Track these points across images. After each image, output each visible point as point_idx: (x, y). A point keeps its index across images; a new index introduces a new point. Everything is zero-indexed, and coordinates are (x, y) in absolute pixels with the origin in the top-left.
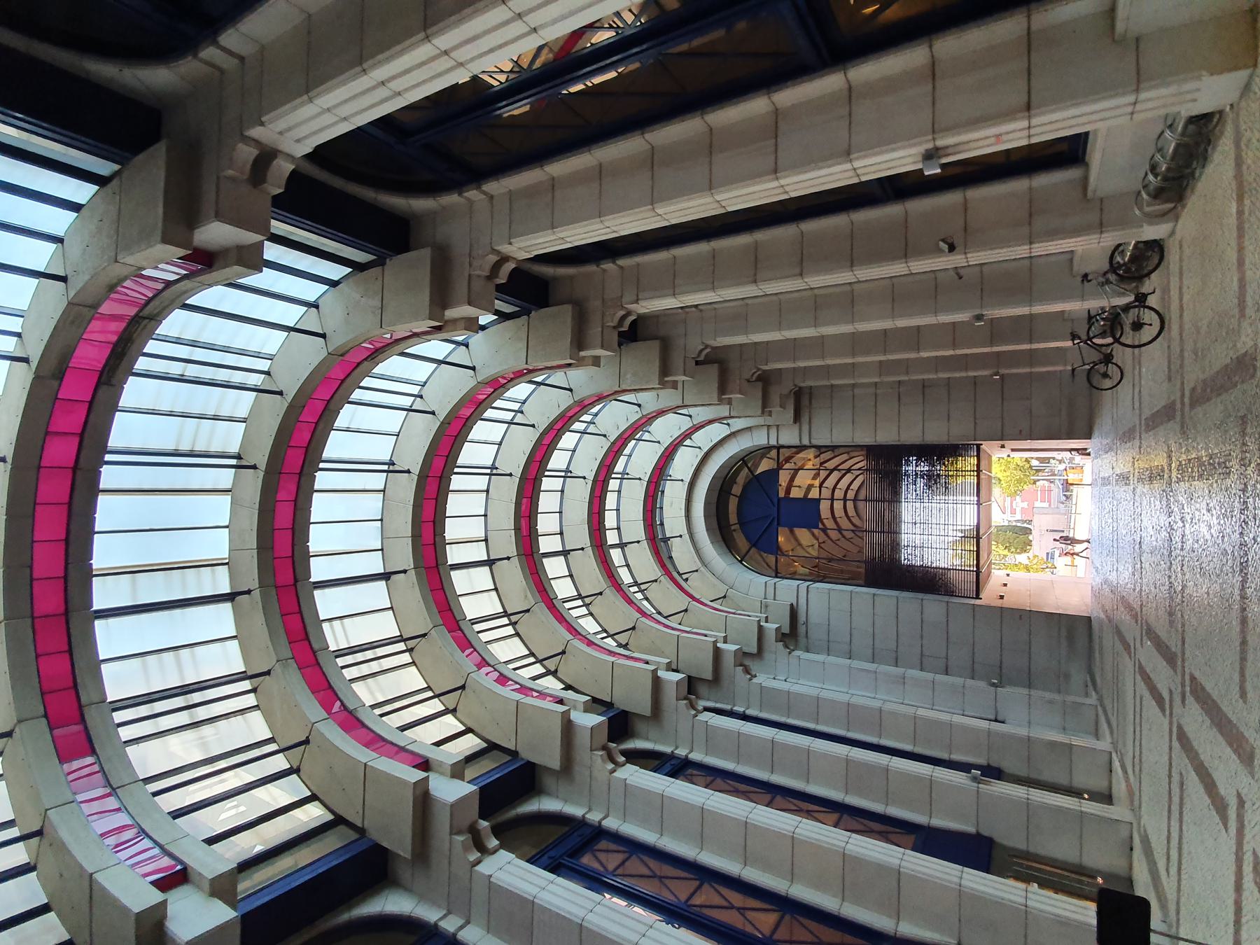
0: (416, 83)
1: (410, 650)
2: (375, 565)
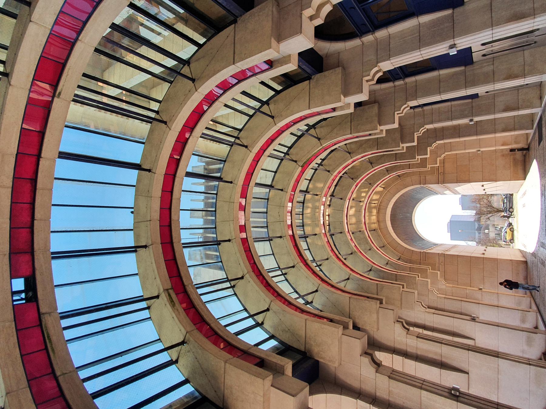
1: (233, 287)
2: (128, 240)
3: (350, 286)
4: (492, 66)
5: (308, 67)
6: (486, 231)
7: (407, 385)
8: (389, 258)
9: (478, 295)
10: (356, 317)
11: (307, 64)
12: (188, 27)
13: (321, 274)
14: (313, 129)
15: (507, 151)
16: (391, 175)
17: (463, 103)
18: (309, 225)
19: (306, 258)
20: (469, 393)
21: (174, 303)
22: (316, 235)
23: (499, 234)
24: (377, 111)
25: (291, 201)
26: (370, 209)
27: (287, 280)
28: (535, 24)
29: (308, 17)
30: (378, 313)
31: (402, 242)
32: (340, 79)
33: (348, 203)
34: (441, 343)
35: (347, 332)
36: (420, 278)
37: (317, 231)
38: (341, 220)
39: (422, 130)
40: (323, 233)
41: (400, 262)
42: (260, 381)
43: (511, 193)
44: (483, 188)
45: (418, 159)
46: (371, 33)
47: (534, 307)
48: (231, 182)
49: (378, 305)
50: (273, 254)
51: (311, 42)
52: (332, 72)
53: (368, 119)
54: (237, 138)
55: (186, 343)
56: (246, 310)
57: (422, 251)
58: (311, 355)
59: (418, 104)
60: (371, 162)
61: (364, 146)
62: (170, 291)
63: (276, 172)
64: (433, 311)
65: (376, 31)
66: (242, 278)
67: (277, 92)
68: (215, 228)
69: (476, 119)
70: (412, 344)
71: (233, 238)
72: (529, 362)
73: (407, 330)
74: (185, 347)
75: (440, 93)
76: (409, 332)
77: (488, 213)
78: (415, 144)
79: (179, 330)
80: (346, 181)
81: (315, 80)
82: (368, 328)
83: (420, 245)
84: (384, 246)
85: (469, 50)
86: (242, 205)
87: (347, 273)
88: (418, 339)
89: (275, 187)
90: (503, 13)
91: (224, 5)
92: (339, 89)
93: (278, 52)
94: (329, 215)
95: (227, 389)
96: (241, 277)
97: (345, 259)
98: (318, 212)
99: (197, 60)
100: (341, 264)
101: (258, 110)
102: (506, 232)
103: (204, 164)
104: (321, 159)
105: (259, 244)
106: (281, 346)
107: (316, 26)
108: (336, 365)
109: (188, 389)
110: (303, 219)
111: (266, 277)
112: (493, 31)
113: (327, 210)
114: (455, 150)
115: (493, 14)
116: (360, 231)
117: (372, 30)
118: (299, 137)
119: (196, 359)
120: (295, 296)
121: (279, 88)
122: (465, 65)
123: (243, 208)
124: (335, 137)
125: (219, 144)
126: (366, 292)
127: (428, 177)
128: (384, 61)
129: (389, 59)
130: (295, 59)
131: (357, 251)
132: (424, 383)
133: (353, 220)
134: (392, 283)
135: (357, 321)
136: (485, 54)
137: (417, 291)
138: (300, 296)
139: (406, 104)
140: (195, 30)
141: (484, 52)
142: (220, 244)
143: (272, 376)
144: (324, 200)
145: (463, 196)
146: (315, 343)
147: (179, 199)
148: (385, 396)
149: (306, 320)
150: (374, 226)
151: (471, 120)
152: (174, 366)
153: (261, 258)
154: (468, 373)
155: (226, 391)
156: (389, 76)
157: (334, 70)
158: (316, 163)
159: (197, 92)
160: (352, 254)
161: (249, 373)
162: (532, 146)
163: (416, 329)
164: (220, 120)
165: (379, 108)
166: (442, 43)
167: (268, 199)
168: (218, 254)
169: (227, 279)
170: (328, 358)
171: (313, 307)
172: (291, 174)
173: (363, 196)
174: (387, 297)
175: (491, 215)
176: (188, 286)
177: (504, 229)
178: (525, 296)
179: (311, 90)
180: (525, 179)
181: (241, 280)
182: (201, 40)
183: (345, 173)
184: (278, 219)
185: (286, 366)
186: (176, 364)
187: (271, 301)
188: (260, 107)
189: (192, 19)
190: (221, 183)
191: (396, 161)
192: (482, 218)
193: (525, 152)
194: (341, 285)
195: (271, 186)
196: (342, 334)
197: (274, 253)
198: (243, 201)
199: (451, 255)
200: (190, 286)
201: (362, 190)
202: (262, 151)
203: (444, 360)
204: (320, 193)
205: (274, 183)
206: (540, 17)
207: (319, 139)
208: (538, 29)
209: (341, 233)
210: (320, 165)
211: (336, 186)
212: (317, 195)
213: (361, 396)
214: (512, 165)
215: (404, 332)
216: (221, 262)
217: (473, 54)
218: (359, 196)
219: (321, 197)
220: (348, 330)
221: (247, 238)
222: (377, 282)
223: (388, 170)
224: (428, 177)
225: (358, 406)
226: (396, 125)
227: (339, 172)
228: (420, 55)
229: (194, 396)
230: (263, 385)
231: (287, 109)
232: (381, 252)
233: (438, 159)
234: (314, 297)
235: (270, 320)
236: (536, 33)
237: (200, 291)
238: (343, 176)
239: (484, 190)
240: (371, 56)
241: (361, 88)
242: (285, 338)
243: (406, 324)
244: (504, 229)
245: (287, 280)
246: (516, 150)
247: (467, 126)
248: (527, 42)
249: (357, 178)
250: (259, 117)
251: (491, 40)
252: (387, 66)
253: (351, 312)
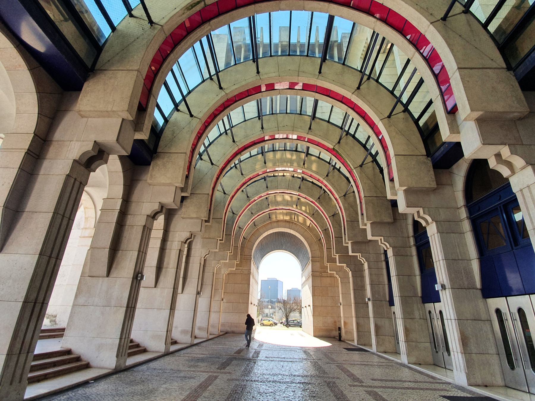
0: (484, 70)
1: (211, 78)
3: (218, 194)
4: (419, 318)
5: (442, 153)
6: (270, 307)
7: (140, 240)
8: (245, 230)
9: (217, 298)
10: (192, 200)
11: (444, 153)
12: (511, 10)
13: (228, 168)
14: (372, 160)
15: (339, 325)
16: (322, 233)
17: (386, 294)
18: (275, 156)
19: (242, 153)
20: (140, 287)
21: (191, 9)
22: (265, 163)
23: (267, 316)
24: (385, 221)
25: (299, 138)
26: (290, 214)
27: (221, 135)
28: (456, 353)
29: (500, 152)
30: (197, 218)
31: (259, 241)
32: (425, 186)
33: (295, 193)
34: (177, 268)
35: (179, 191)
36: (229, 254)
37: (269, 164)
38: (279, 187)
39: (363, 260)
40: (267, 170)
41: (241, 239)
42: (126, 107)
43: (302, 326)
44: (307, 306)
45: (336, 256)
46: (468, 216)
47: (211, 337)
48: (320, 72)
49: (204, 219)
50: (245, 121)
51: (471, 154)
52: (432, 178)
53: (378, 213)
54: (369, 77)
55: (152, 26)
56: (189, 92)
57: (252, 257)
58: (154, 158)
59: (388, 257)
60: (334, 216)
61: (351, 209)
62: (203, 3)
63: (328, 122)
64: (202, 263)
65: (470, 221)
66: (221, 88)
67: (416, 121)
68: (271, 56)
69: (370, 304)
70: (173, 245)
71: (260, 76)
72: (169, 331)
73: (185, 242)
74: (147, 25)
75: (398, 275)
76: (183, 244)
77: (285, 308)
78: (350, 253)
79: (164, 16)
80: (317, 193)
81: (425, 160)
82: (183, 210)
83: (257, 256)
84: (255, 225)
85: (437, 300)
86: (294, 86)
87: (229, 193)
88: (179, 251)
89: (313, 122)
90: (469, 329)
91: (532, 55)
92: (414, 185)
93: (465, 119)
94: (284, 176)
95: (113, 73)
96: (222, 86)
97: (242, 191)
98: (287, 165)
99: (468, 22)
100: (238, 187)
101: (399, 100)
102: (269, 321)
103: (339, 41)
104: (340, 167)
105: (255, 106)
106: (159, 130)
107: (488, 161)
108: (149, 181)
109: (106, 31)
110: (279, 150)
111: (223, 113)
112: (454, 320)
113: (288, 174)
114: (342, 286)
115: (471, 321)
116: (269, 205)
117: (471, 217)
118: (364, 146)
119: (136, 38)
120: (207, 143)
121: (421, 123)
122: (422, 297)
123: (292, 86)
124: (362, 182)
125: (361, 58)
126: (214, 209)
127: (318, 264)
128: (437, 228)
129: (438, 231)
130: (454, 139)
131: (250, 201)
132: (144, 254)
133: (279, 199)
134: (223, 231)
135: (188, 201)
136: (431, 313)
137: (218, 251)
138: (206, 148)
139: (390, 246)
140: (506, 19)
141: (433, 312)
142: (254, 62)
143: (132, 119)
144: (299, 171)
145: (299, 291)
146: (165, 162)
147: (304, 9)
148: (128, 222)
149: (185, 153)
150: (274, 217)
151: (369, 299)
152: (126, 13)
153: (241, 108)
154: (155, 287)
155: (111, 72)
156: (420, 232)
157: (434, 180)
158: (336, 163)
159: (429, 23)
160: (248, 197)
161: (131, 97)
162: (342, 343)
163: (186, 250)
164: (390, 58)
165: (389, 223)
166: (448, 278)
167: (301, 114)
168: (242, 61)
169: (218, 71)
170: (154, 173)
171: (197, 161)
172: (326, 138)
173: (302, 208)
174: (211, 226)
175: (284, 311)
176: (209, 25)
177: (272, 320)
178: (219, 331)
179: (415, 157)
180: (314, 336)
181: (218, 86)
182: (492, 27)
183: (325, 191)
184: (281, 125)
185: (143, 134)
186: (128, 16)
187: (200, 119)
188: (402, 103)
189: (521, 14)
190: (319, 61)
191: (335, 237)
192: (281, 304)
193: (338, 338)
194: (219, 187)
195: (314, 117)
196: (176, 187)
197: (247, 122)
198: (299, 87)
199: (250, 279)
200: (209, 27)
201: (308, 207)
202: (352, 106)
203: (164, 270)
204: (306, 167)
205: (318, 120)
206: (462, 357)
207: (361, 166)
208: (449, 354)
209: (267, 187)
210: (334, 167)
211: (312, 182)
212: (304, 164)
213: (126, 202)
214: (327, 328)
215: (183, 239)
216: (236, 64)
217: (433, 303)
218: (302, 204)
219: (302, 168)
220: (180, 192)
221: (261, 92)
222: (223, 219)
223: (326, 231)
224: (318, 264)
225: (116, 200)
226: (370, 237)
227: (326, 186)
228: (439, 259)
229: (100, 38)
230: (123, 111)
231: (397, 133)
232: (250, 222)
233: (335, 272)
234: (207, 162)
235: (181, 118)
236: (446, 354)
237: (204, 40)
238: (322, 189)
239: (306, 307)
240: (443, 215)
241: (411, 206)
242: (167, 133)
243: (190, 242)
244: (272, 320)
245: (221, 135)
246: (340, 332)
247: (364, 296)
248: (438, 346)
249: (320, 203)
250: (390, 102)
251: (445, 317)
252: (432, 231)
253: (195, 195)
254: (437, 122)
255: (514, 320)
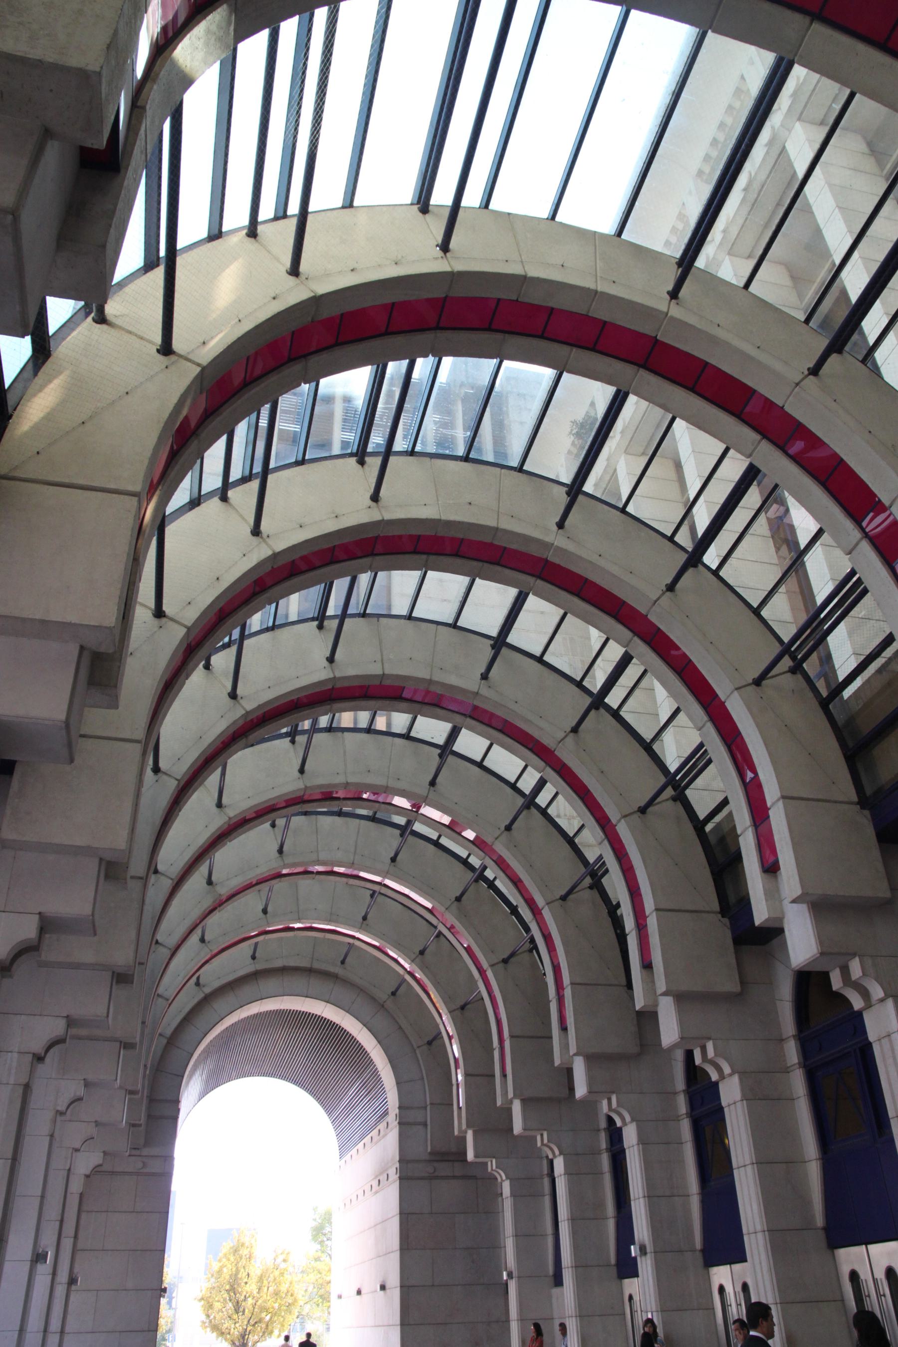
210: (481, 877)
252: (630, 1136)
254: (740, 848)
255: (881, 1296)
